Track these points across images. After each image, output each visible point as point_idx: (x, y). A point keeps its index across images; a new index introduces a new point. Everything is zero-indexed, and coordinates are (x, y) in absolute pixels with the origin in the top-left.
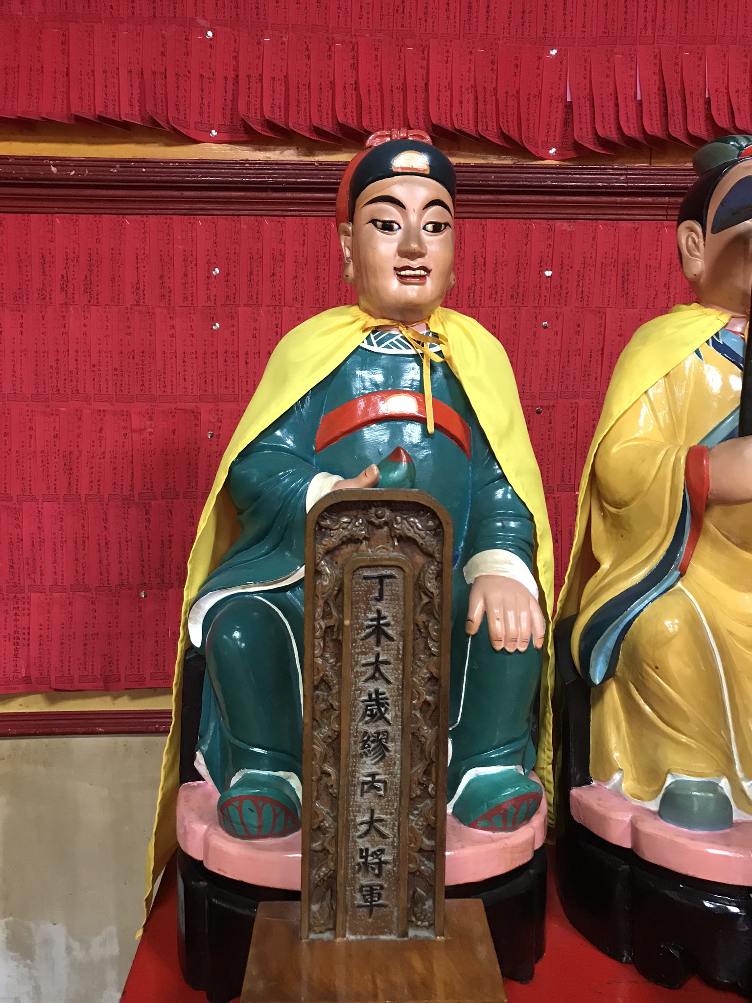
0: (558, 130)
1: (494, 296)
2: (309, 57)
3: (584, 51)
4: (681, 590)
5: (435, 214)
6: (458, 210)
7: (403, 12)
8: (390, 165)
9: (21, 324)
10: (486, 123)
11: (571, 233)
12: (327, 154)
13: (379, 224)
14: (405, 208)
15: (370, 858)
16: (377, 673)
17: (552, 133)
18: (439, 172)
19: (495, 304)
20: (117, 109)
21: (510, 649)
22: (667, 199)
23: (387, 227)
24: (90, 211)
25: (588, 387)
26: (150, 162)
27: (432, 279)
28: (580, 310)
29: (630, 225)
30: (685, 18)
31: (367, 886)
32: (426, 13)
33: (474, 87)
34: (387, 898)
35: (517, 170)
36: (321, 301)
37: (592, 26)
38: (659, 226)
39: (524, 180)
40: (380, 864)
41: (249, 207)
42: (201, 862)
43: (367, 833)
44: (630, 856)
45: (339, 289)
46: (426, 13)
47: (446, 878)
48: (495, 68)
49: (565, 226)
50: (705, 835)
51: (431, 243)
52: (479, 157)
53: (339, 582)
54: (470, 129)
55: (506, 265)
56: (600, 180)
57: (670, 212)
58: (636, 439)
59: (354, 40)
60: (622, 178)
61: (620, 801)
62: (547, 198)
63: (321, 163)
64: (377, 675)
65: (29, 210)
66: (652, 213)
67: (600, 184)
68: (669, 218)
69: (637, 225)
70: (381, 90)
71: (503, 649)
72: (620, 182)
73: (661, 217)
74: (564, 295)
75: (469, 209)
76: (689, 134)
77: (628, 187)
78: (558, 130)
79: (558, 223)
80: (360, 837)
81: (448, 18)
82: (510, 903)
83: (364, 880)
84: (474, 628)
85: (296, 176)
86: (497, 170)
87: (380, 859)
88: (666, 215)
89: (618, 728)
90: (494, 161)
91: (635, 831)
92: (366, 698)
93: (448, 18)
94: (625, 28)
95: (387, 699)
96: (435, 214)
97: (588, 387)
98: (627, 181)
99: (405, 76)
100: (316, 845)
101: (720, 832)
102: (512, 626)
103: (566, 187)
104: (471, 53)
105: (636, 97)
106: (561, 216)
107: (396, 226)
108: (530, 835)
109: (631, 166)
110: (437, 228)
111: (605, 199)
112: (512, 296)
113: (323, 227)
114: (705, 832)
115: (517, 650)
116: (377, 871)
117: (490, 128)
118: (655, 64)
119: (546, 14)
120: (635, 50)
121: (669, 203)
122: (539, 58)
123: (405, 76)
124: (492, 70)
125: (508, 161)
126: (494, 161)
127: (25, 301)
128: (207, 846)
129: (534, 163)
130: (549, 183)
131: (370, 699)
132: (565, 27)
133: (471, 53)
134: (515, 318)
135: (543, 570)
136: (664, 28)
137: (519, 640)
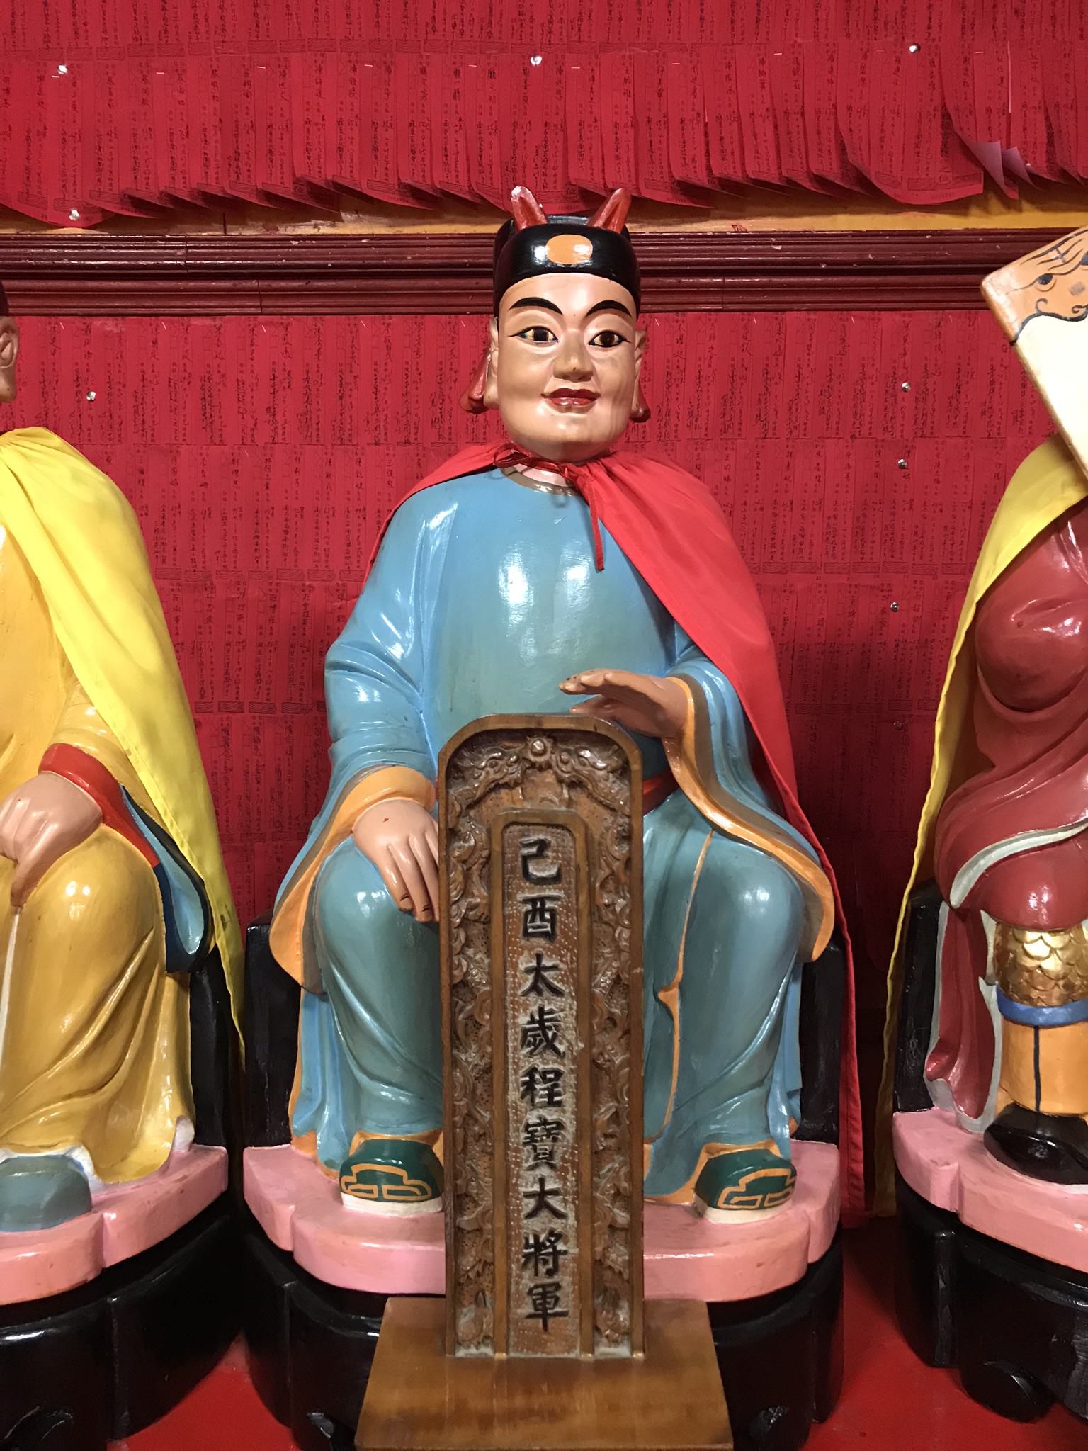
3: (107, 67)
5: (605, 322)
11: (120, 335)
13: (530, 333)
14: (559, 311)
16: (540, 985)
17: (70, 186)
18: (613, 259)
20: (428, 175)
22: (254, 283)
23: (541, 335)
25: (164, 561)
28: (142, 449)
29: (208, 321)
30: (255, 14)
35: (19, 243)
37: (116, 30)
38: (252, 323)
39: (30, 256)
40: (556, 1254)
42: (291, 1254)
47: (648, 1280)
49: (110, 325)
51: (601, 361)
56: (143, 256)
60: (180, 253)
62: (73, 284)
66: (237, 303)
67: (144, 263)
68: (265, 310)
69: (218, 321)
72: (176, 258)
73: (253, 310)
74: (116, 426)
77: (187, 267)
79: (97, 322)
80: (529, 1216)
82: (769, 1347)
87: (555, 1248)
88: (261, 307)
94: (166, 31)
96: (605, 322)
97: (164, 561)
98: (187, 257)
99: (805, 127)
103: (93, 267)
106: (102, 311)
107: (551, 336)
109: (192, 235)
110: (607, 339)
111: (161, 284)
116: (551, 1266)
120: (183, 64)
121: (257, 289)
122: (41, 78)
123: (805, 127)
127: (641, 435)
128: (294, 1233)
129: (49, 232)
130: (65, 261)
131: (532, 1021)
132: (76, 33)
136: (223, 30)
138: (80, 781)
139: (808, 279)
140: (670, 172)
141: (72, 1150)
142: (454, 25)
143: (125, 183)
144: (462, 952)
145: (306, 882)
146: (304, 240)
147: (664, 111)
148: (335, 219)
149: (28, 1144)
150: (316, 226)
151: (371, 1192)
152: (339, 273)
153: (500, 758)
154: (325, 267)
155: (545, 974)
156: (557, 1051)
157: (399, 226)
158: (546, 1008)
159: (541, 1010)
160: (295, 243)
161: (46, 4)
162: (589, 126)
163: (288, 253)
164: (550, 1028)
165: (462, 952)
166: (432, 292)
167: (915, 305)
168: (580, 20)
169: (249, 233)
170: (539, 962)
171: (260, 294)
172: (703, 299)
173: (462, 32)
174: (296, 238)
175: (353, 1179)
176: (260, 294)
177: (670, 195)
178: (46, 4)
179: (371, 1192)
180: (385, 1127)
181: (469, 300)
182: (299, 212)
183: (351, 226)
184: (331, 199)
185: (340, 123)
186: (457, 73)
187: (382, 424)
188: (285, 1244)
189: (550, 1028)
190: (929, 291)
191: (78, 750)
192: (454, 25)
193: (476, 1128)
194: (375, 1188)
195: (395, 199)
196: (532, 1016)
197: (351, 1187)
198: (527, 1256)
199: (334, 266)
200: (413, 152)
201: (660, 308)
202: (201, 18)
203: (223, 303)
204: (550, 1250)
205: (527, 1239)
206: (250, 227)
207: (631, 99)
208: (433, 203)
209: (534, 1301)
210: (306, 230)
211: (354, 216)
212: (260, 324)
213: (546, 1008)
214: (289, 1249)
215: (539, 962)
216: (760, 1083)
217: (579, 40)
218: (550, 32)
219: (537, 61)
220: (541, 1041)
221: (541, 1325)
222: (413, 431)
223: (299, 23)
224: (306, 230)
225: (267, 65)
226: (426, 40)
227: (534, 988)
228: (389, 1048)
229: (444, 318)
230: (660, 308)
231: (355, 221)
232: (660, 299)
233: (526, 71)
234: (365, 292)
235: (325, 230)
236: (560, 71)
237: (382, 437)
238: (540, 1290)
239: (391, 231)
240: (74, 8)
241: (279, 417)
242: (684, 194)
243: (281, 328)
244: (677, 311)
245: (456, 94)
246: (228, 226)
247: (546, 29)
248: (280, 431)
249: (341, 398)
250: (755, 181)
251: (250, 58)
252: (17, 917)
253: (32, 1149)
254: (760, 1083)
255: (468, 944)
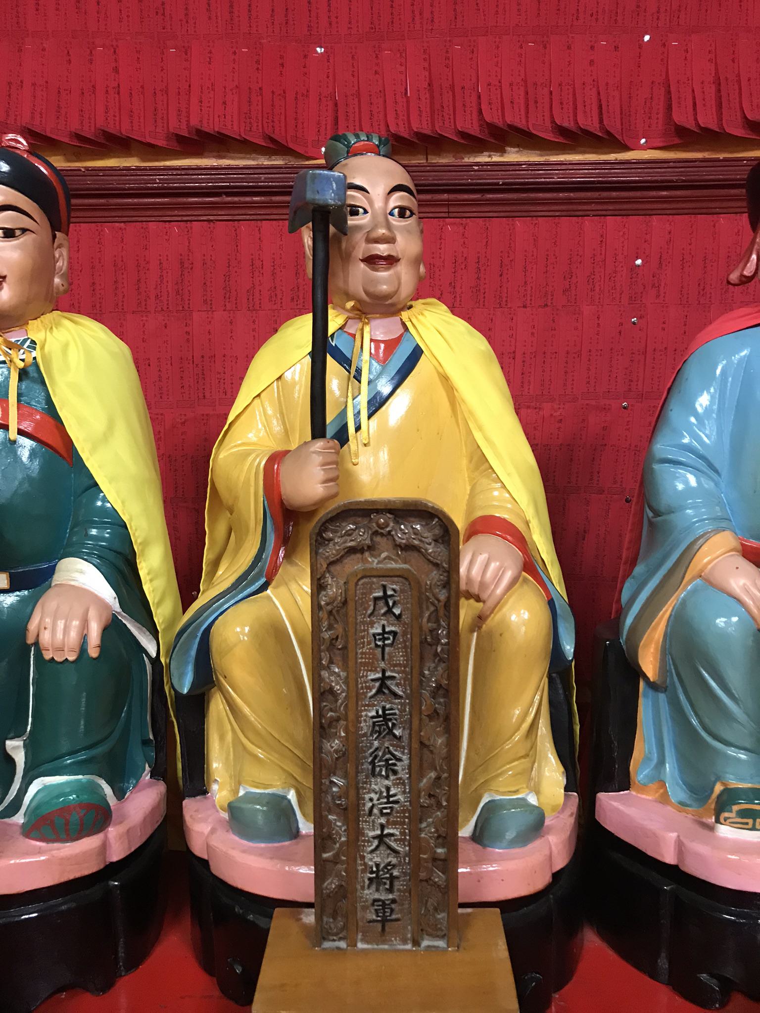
0: (329, 127)
1: (273, 299)
2: (70, 62)
4: (269, 598)
6: (423, 210)
7: (163, 14)
8: (10, 171)
9: (685, 325)
10: (250, 123)
12: (685, 151)
15: (381, 873)
19: (275, 307)
21: (58, 659)
22: (445, 196)
24: (663, 212)
26: (657, 162)
27: (9, 284)
31: (379, 900)
32: (186, 15)
33: (525, 81)
34: (401, 911)
36: (98, 306)
37: (357, 22)
38: (441, 223)
40: (392, 878)
41: (156, 213)
43: (377, 847)
44: (674, 873)
45: (116, 294)
46: (186, 15)
48: (260, 67)
50: (262, 848)
52: (248, 159)
53: (475, 590)
54: (593, 126)
55: (284, 267)
57: (452, 209)
58: (243, 444)
59: (114, 43)
61: (648, 814)
63: (87, 169)
64: (386, 691)
65: (103, 220)
70: (739, 82)
71: (53, 658)
75: (243, 212)
76: (581, 128)
78: (329, 127)
81: (210, 18)
82: (538, 930)
83: (370, 894)
84: (30, 640)
85: (242, 180)
86: (267, 171)
87: (391, 874)
88: (449, 212)
89: (222, 738)
90: (265, 162)
91: (680, 847)
92: (374, 713)
93: (210, 18)
95: (395, 714)
100: (325, 855)
101: (276, 845)
102: (60, 635)
104: (235, 53)
105: (406, 93)
107: (361, 210)
108: (554, 849)
112: (293, 299)
113: (97, 233)
114: (263, 845)
115: (53, 658)
116: (387, 887)
117: (254, 128)
118: (425, 60)
119: (310, 11)
121: (448, 200)
122: (305, 56)
124: (258, 69)
125: (278, 162)
126: (265, 162)
131: (378, 716)
132: (330, 24)
133: (235, 53)
134: (231, 323)
135: (148, 578)
136: (432, 21)
137: (66, 649)
138: (508, 537)
139: (236, 199)
140: (552, 117)
141: (527, 795)
142: (592, 15)
143: (75, 126)
144: (328, 668)
145: (667, 611)
146: (482, 165)
147: (236, 83)
148: (503, 151)
149: (501, 790)
150: (490, 156)
151: (747, 824)
152: (508, 188)
153: (354, 530)
154: (498, 184)
155: (389, 683)
156: (395, 736)
157: (548, 155)
158: (388, 706)
159: (384, 709)
160: (476, 168)
161: (309, 3)
162: (684, 83)
163: (471, 175)
164: (390, 720)
165: (328, 668)
166: (569, 201)
167: (674, 212)
168: (679, 11)
169: (444, 160)
170: (382, 831)
171: (448, 204)
172: (539, 208)
173: (597, 20)
174: (477, 164)
175: (733, 815)
176: (448, 204)
177: (743, 131)
178: (309, 3)
179: (747, 824)
180: (742, 780)
181: (593, 207)
182: (477, 144)
183: (513, 156)
184: (501, 137)
185: (511, 85)
186: (592, 48)
187: (529, 292)
188: (670, 858)
189: (390, 720)
190: (691, 201)
191: (504, 520)
192: (592, 15)
193: (334, 789)
194: (750, 821)
195: (550, 136)
196: (377, 712)
197: (728, 821)
198: (370, 879)
199: (503, 184)
200: (561, 103)
201: (725, 211)
202: (417, 13)
203: (207, 212)
204: (388, 875)
205: (372, 868)
206: (443, 158)
207: (713, 65)
208: (573, 138)
209: (376, 910)
210: (483, 158)
211: (516, 149)
212: (447, 224)
213: (388, 706)
214: (206, 857)
215: (382, 831)
216: (526, 756)
217: (678, 24)
218: (658, 19)
219: (647, 38)
220: (384, 730)
221: (380, 929)
222: (550, 297)
223: (485, 15)
224: (483, 158)
225: (461, 45)
226: (572, 26)
227: (380, 691)
228: (263, 732)
229: (481, 221)
230: (725, 211)
231: (517, 152)
232: (725, 204)
233: (640, 47)
234: (523, 202)
235: (496, 158)
236: (664, 45)
237: (529, 302)
238: (380, 903)
239: (541, 159)
240: (329, 5)
241: (458, 289)
242: (752, 130)
243: (461, 228)
244: (736, 213)
245: (592, 62)
246: (429, 157)
247: (655, 17)
248: (458, 299)
249: (501, 275)
250: (510, 126)
251: (450, 41)
252: (475, 634)
253: (504, 793)
254: (526, 756)
255: (331, 662)
